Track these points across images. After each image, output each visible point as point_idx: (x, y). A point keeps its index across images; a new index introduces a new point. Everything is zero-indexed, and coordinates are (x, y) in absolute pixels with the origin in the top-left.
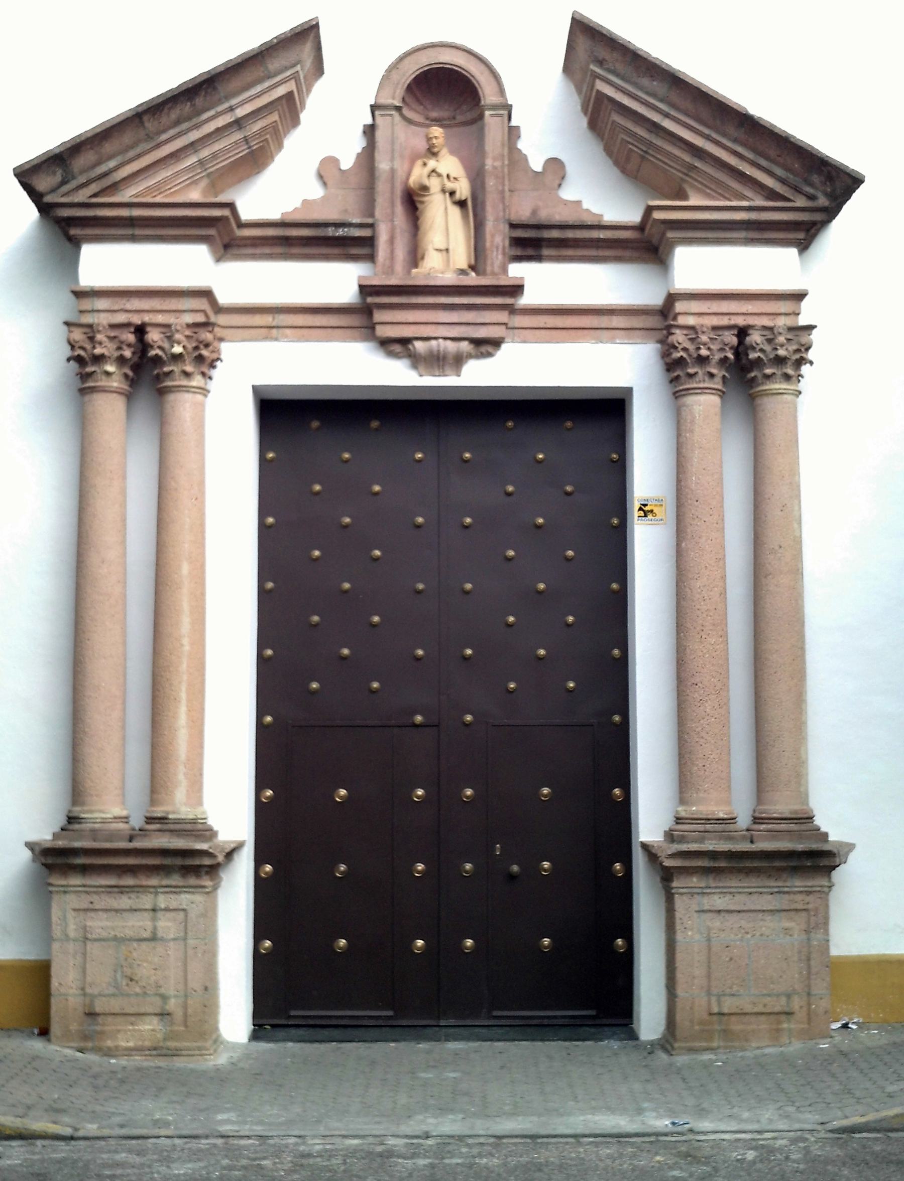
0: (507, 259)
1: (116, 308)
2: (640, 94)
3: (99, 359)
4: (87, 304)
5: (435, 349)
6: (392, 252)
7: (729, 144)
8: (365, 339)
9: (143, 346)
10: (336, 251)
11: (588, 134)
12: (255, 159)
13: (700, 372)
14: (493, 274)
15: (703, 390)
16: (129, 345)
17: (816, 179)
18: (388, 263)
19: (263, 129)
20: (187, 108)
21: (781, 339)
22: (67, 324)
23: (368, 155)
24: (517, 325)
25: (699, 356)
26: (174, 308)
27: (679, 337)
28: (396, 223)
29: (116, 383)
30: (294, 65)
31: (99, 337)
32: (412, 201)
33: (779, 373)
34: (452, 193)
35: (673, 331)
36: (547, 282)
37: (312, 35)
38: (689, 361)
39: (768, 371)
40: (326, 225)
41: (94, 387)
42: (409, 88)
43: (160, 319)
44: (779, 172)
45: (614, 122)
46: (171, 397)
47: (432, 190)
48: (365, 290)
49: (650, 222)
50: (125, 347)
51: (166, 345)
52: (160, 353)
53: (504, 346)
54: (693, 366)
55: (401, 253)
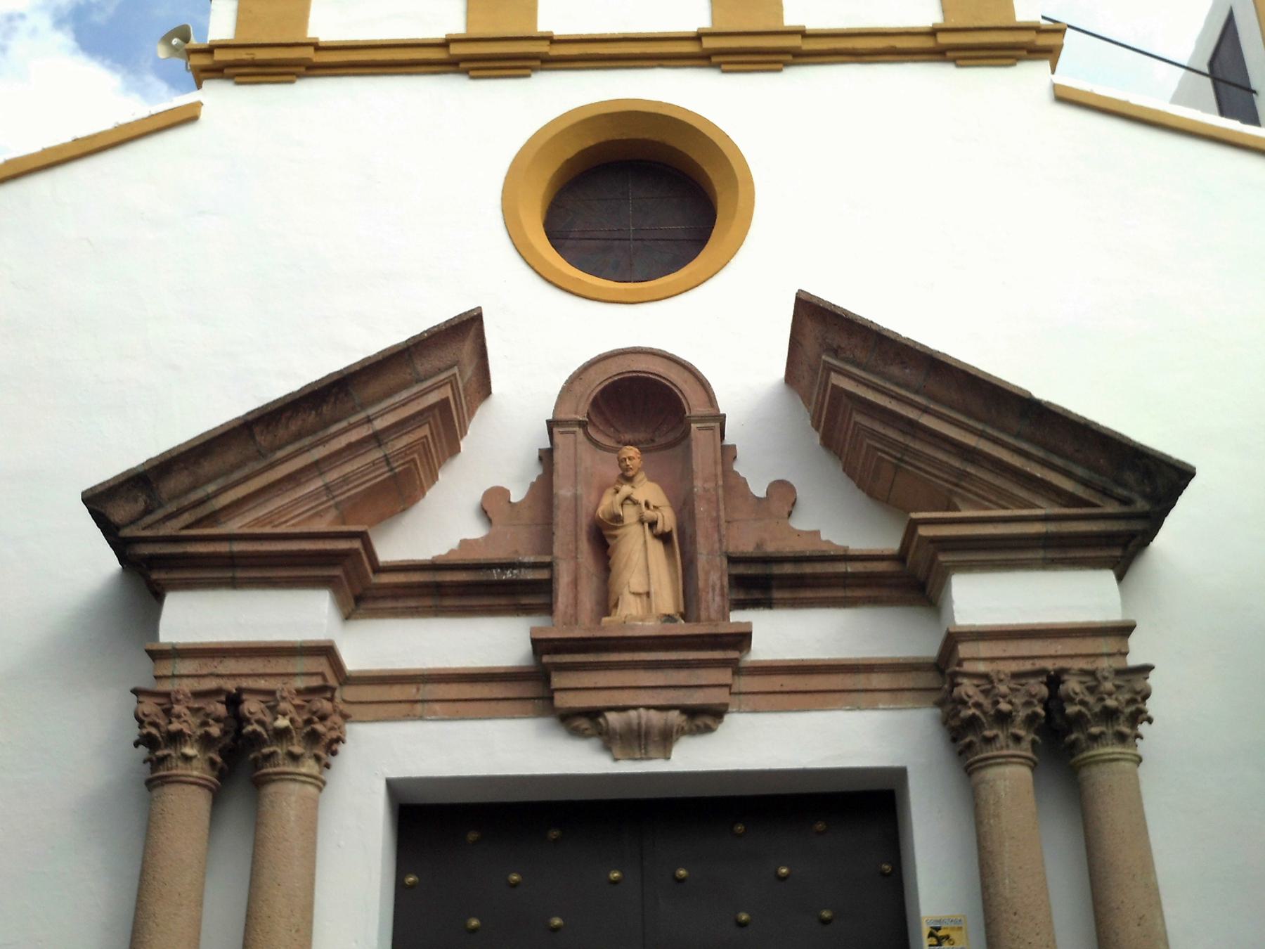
0: (727, 606)
1: (204, 672)
2: (888, 385)
3: (176, 738)
4: (166, 668)
5: (635, 722)
6: (576, 598)
7: (1011, 440)
8: (538, 714)
9: (236, 717)
10: (503, 601)
11: (822, 452)
12: (402, 489)
13: (1001, 736)
14: (709, 620)
15: (1008, 760)
16: (217, 720)
17: (1130, 477)
18: (570, 611)
19: (409, 446)
20: (312, 418)
21: (1108, 686)
22: (136, 692)
23: (544, 489)
24: (744, 689)
25: (999, 712)
26: (282, 670)
27: (967, 688)
28: (580, 560)
29: (198, 770)
30: (451, 367)
31: (177, 708)
32: (602, 537)
33: (1110, 732)
34: (653, 524)
35: (960, 680)
36: (779, 634)
37: (472, 333)
38: (984, 720)
39: (1095, 730)
40: (489, 566)
41: (166, 776)
42: (595, 404)
43: (262, 684)
44: (1080, 471)
45: (856, 423)
46: (271, 789)
47: (627, 521)
48: (540, 646)
49: (916, 539)
50: (211, 722)
51: (268, 719)
52: (259, 729)
53: (727, 718)
54: (991, 728)
55: (588, 600)
